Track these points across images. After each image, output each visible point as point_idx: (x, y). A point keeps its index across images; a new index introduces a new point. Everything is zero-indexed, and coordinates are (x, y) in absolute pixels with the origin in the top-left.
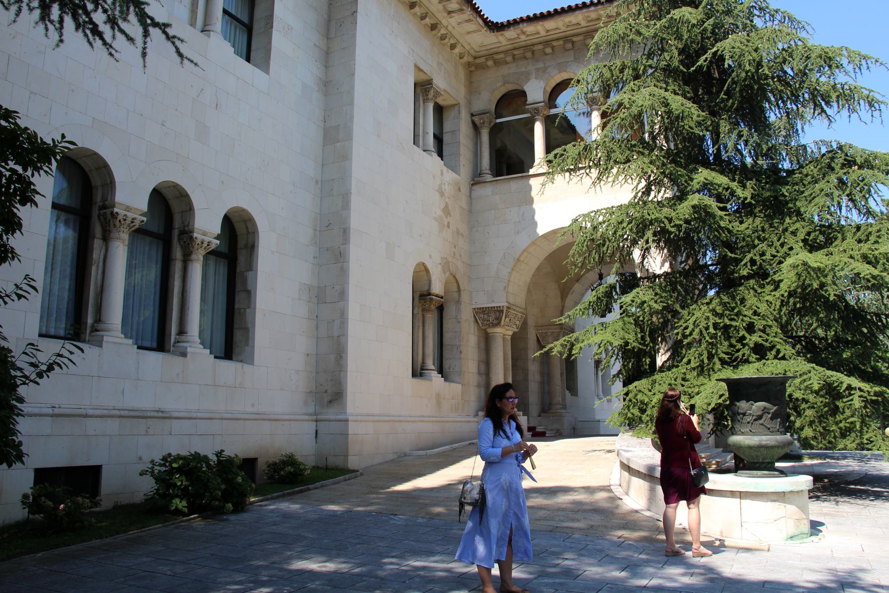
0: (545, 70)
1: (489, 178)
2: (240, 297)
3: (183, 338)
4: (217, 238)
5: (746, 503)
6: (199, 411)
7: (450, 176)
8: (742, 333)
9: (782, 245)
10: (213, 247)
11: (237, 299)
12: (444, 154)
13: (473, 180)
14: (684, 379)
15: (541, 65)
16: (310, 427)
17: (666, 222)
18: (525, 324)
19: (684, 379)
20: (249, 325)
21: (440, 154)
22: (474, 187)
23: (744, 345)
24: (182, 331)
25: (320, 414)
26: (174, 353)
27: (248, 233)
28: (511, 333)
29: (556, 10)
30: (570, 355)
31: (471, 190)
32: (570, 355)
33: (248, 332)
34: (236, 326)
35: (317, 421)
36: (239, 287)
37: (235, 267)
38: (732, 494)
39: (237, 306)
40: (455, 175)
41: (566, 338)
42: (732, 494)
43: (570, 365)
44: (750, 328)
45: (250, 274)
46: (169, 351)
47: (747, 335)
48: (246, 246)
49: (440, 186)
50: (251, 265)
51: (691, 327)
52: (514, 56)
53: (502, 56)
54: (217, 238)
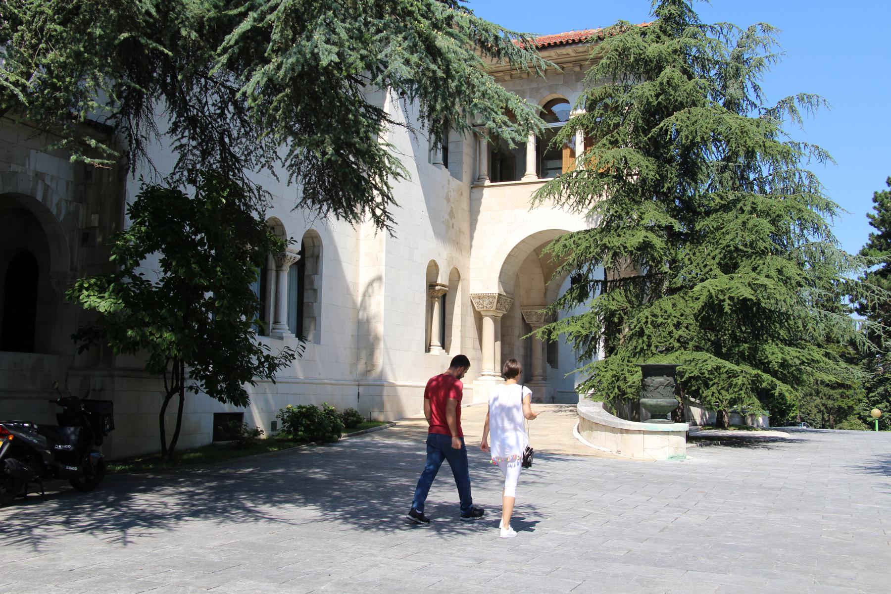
0: (538, 90)
1: (487, 183)
2: (308, 294)
3: (278, 326)
4: (298, 254)
5: (646, 436)
6: (290, 378)
7: (455, 183)
8: (672, 328)
9: (705, 266)
10: (297, 260)
11: (305, 295)
12: (449, 161)
13: (473, 183)
14: (628, 361)
15: (534, 85)
16: (354, 390)
17: (622, 248)
18: (513, 306)
19: (628, 361)
20: (316, 315)
21: (446, 164)
22: (474, 190)
23: (671, 337)
24: (276, 322)
25: (361, 380)
26: (272, 337)
27: (314, 246)
28: (501, 315)
29: (549, 44)
30: (549, 339)
31: (471, 193)
32: (549, 339)
33: (315, 319)
34: (305, 315)
35: (359, 385)
36: (307, 286)
37: (304, 271)
38: (640, 432)
39: (305, 300)
40: (459, 182)
41: (546, 326)
42: (640, 432)
43: (551, 348)
44: (678, 326)
45: (316, 277)
46: (268, 335)
47: (675, 331)
48: (312, 256)
49: (447, 194)
50: (317, 270)
51: (635, 322)
52: (511, 75)
53: (502, 74)
54: (298, 254)
